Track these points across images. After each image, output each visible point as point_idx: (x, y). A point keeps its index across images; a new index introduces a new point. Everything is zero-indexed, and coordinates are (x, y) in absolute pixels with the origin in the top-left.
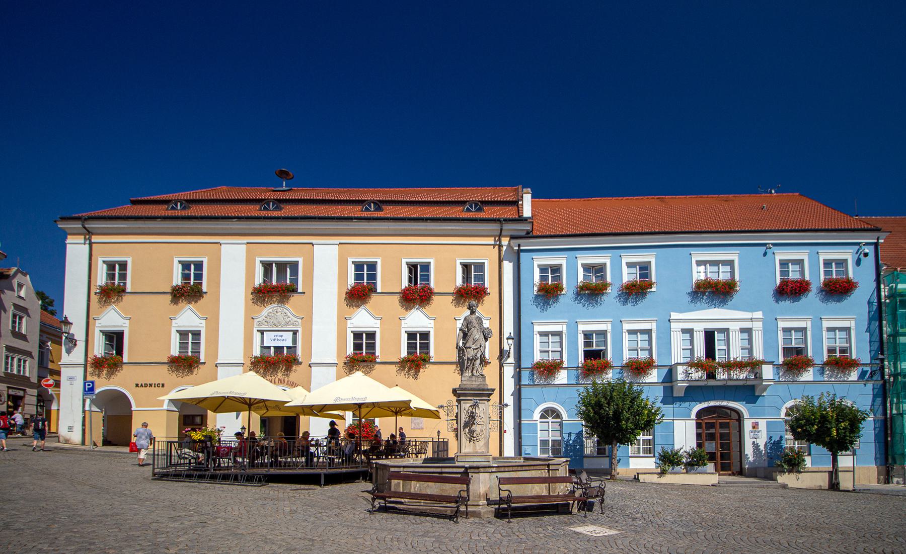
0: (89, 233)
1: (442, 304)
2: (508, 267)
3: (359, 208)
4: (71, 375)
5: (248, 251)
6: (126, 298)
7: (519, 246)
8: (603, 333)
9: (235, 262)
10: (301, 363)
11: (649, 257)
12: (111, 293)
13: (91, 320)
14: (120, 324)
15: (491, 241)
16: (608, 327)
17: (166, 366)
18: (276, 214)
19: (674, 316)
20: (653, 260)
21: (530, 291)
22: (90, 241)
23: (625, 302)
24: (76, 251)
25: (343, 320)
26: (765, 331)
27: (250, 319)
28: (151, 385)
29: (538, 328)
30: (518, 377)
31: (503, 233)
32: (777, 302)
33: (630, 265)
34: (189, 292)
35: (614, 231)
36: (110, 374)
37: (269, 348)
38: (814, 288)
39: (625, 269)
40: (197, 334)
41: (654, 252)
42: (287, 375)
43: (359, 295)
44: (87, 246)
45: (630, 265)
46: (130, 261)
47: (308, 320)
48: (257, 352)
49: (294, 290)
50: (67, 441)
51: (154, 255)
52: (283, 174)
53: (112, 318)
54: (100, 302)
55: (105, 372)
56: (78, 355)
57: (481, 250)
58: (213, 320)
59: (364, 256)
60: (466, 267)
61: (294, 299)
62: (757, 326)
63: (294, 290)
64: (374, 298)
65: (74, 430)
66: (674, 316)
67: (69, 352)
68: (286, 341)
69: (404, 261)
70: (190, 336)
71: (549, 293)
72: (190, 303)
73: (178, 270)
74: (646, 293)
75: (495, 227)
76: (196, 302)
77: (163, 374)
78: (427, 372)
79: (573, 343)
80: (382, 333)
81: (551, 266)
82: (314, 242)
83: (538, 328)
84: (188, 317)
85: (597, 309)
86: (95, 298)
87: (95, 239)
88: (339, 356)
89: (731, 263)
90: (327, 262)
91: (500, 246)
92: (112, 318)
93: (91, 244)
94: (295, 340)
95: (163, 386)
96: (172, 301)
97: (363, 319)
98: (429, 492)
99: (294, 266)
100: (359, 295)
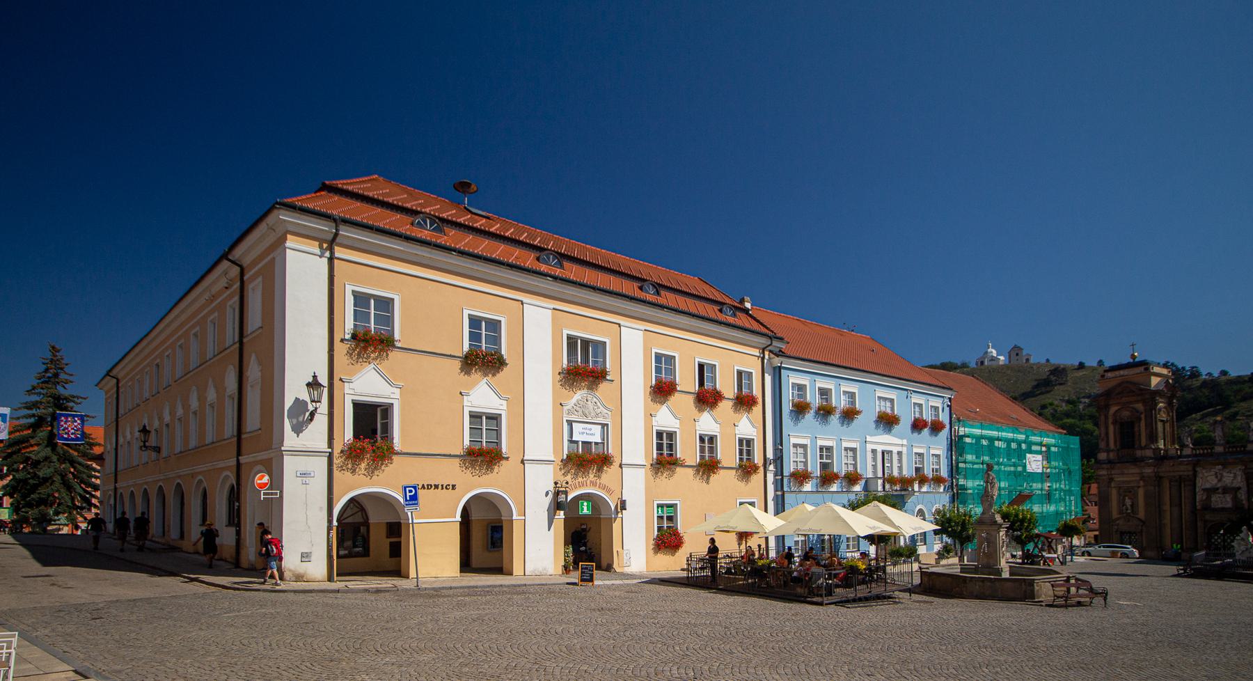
0: (331, 243)
2: (768, 378)
4: (303, 469)
5: (554, 319)
6: (394, 354)
9: (539, 328)
10: (507, 459)
12: (372, 342)
13: (336, 382)
14: (497, 406)
15: (757, 352)
17: (458, 460)
18: (731, 320)
19: (869, 438)
21: (787, 407)
22: (332, 253)
23: (842, 424)
24: (304, 269)
26: (908, 454)
28: (436, 487)
30: (779, 485)
31: (338, 240)
32: (842, 424)
34: (484, 359)
35: (257, 217)
36: (371, 471)
37: (577, 442)
38: (838, 411)
39: (843, 397)
40: (495, 418)
42: (599, 477)
44: (325, 261)
46: (503, 320)
50: (299, 578)
51: (434, 300)
52: (463, 187)
53: (368, 383)
54: (350, 354)
55: (363, 465)
56: (316, 435)
58: (518, 402)
59: (665, 348)
60: (475, 322)
61: (603, 386)
62: (904, 450)
65: (313, 558)
66: (869, 438)
67: (298, 429)
68: (594, 435)
69: (466, 313)
70: (485, 421)
71: (800, 409)
72: (486, 375)
75: (325, 227)
76: (494, 375)
77: (452, 471)
80: (402, 409)
81: (378, 299)
82: (622, 323)
83: (793, 441)
84: (482, 395)
86: (341, 349)
87: (339, 252)
88: (555, 452)
89: (892, 401)
90: (633, 345)
91: (763, 359)
92: (368, 383)
93: (331, 260)
94: (605, 435)
95: (454, 487)
96: (462, 369)
97: (665, 418)
99: (494, 325)
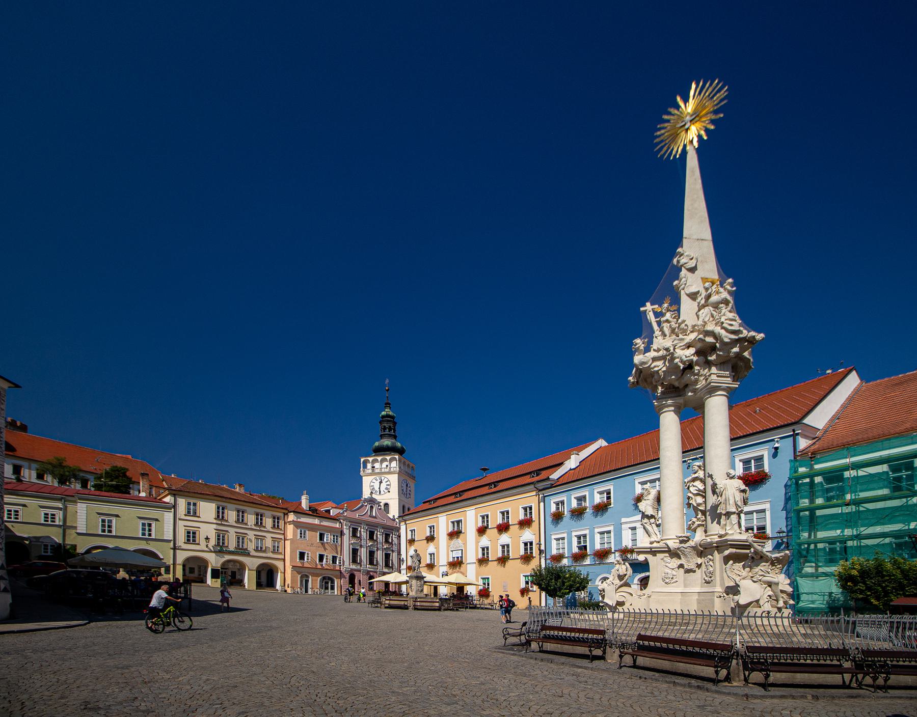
0: (405, 521)
1: (492, 532)
2: (542, 504)
3: (529, 476)
7: (794, 431)
8: (585, 536)
11: (610, 486)
16: (587, 532)
19: (623, 520)
20: (612, 488)
23: (596, 516)
25: (477, 542)
27: (448, 546)
29: (553, 537)
33: (601, 493)
34: (431, 539)
41: (612, 482)
43: (482, 531)
45: (601, 493)
47: (465, 544)
48: (451, 560)
49: (461, 532)
57: (530, 499)
58: (437, 548)
61: (462, 535)
63: (461, 532)
64: (488, 531)
71: (558, 517)
73: (522, 512)
74: (607, 509)
78: (509, 564)
79: (570, 543)
83: (553, 537)
84: (431, 548)
85: (582, 522)
90: (471, 517)
97: (485, 541)
98: (577, 652)
100: (482, 531)
